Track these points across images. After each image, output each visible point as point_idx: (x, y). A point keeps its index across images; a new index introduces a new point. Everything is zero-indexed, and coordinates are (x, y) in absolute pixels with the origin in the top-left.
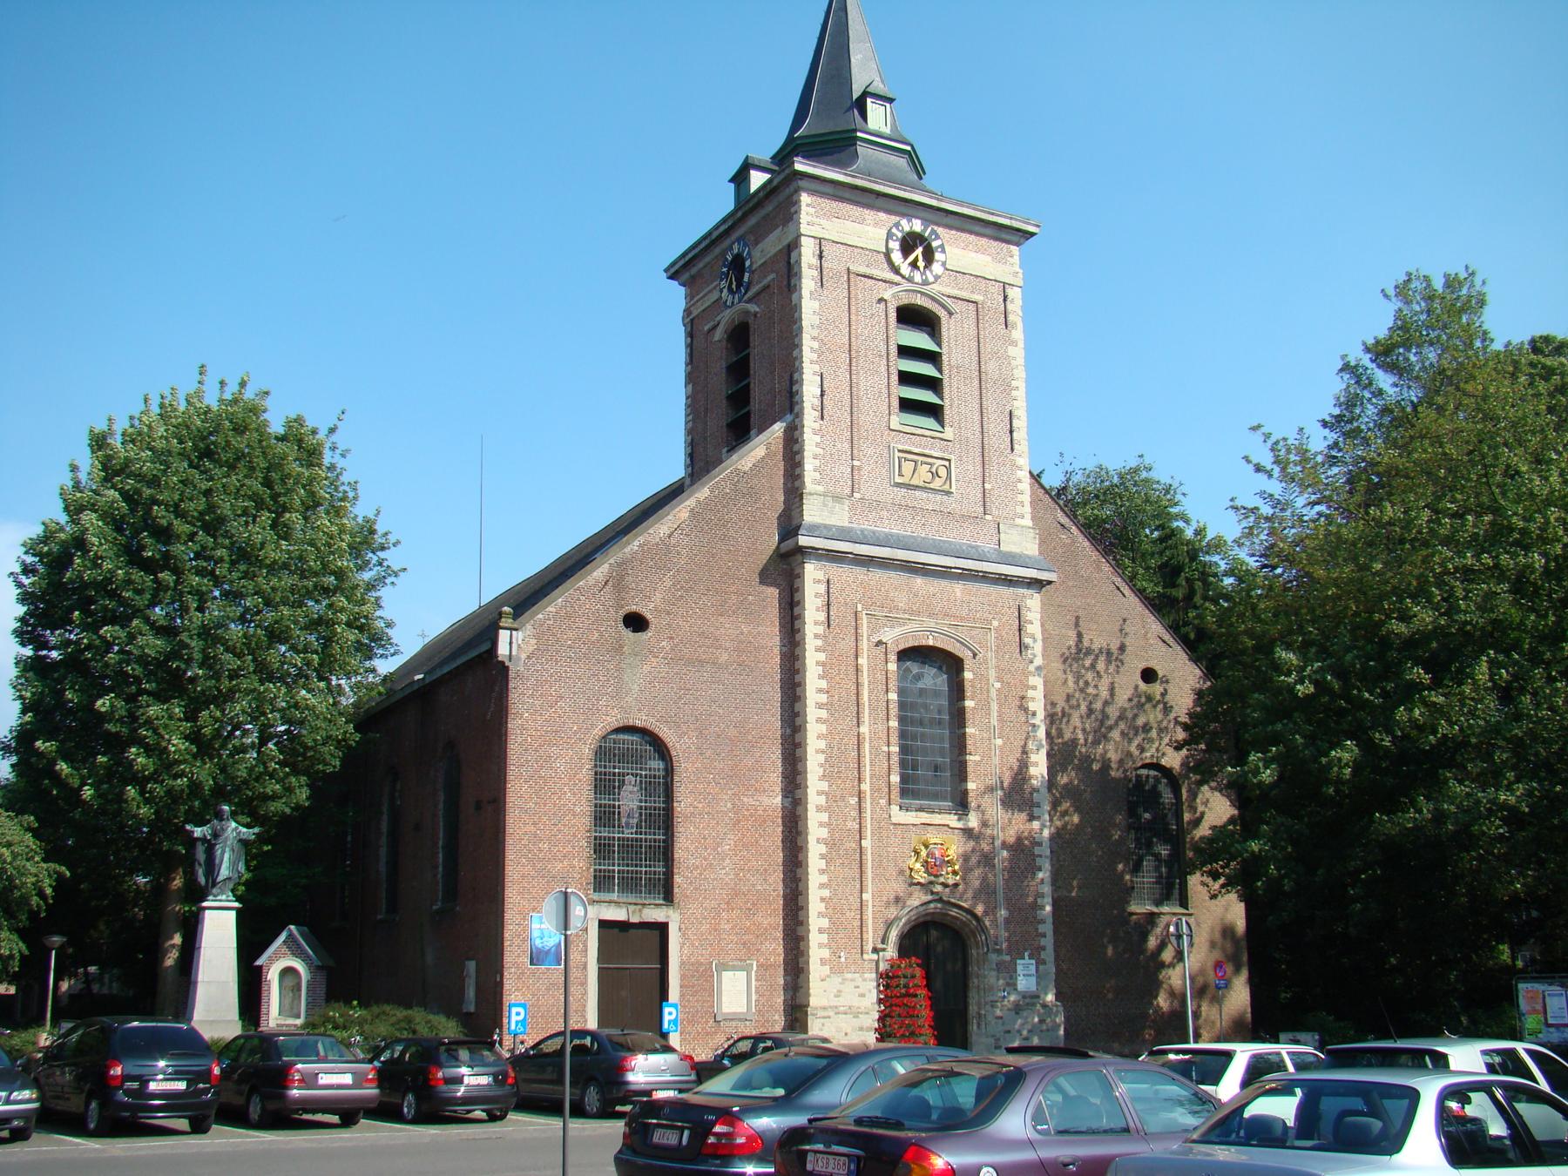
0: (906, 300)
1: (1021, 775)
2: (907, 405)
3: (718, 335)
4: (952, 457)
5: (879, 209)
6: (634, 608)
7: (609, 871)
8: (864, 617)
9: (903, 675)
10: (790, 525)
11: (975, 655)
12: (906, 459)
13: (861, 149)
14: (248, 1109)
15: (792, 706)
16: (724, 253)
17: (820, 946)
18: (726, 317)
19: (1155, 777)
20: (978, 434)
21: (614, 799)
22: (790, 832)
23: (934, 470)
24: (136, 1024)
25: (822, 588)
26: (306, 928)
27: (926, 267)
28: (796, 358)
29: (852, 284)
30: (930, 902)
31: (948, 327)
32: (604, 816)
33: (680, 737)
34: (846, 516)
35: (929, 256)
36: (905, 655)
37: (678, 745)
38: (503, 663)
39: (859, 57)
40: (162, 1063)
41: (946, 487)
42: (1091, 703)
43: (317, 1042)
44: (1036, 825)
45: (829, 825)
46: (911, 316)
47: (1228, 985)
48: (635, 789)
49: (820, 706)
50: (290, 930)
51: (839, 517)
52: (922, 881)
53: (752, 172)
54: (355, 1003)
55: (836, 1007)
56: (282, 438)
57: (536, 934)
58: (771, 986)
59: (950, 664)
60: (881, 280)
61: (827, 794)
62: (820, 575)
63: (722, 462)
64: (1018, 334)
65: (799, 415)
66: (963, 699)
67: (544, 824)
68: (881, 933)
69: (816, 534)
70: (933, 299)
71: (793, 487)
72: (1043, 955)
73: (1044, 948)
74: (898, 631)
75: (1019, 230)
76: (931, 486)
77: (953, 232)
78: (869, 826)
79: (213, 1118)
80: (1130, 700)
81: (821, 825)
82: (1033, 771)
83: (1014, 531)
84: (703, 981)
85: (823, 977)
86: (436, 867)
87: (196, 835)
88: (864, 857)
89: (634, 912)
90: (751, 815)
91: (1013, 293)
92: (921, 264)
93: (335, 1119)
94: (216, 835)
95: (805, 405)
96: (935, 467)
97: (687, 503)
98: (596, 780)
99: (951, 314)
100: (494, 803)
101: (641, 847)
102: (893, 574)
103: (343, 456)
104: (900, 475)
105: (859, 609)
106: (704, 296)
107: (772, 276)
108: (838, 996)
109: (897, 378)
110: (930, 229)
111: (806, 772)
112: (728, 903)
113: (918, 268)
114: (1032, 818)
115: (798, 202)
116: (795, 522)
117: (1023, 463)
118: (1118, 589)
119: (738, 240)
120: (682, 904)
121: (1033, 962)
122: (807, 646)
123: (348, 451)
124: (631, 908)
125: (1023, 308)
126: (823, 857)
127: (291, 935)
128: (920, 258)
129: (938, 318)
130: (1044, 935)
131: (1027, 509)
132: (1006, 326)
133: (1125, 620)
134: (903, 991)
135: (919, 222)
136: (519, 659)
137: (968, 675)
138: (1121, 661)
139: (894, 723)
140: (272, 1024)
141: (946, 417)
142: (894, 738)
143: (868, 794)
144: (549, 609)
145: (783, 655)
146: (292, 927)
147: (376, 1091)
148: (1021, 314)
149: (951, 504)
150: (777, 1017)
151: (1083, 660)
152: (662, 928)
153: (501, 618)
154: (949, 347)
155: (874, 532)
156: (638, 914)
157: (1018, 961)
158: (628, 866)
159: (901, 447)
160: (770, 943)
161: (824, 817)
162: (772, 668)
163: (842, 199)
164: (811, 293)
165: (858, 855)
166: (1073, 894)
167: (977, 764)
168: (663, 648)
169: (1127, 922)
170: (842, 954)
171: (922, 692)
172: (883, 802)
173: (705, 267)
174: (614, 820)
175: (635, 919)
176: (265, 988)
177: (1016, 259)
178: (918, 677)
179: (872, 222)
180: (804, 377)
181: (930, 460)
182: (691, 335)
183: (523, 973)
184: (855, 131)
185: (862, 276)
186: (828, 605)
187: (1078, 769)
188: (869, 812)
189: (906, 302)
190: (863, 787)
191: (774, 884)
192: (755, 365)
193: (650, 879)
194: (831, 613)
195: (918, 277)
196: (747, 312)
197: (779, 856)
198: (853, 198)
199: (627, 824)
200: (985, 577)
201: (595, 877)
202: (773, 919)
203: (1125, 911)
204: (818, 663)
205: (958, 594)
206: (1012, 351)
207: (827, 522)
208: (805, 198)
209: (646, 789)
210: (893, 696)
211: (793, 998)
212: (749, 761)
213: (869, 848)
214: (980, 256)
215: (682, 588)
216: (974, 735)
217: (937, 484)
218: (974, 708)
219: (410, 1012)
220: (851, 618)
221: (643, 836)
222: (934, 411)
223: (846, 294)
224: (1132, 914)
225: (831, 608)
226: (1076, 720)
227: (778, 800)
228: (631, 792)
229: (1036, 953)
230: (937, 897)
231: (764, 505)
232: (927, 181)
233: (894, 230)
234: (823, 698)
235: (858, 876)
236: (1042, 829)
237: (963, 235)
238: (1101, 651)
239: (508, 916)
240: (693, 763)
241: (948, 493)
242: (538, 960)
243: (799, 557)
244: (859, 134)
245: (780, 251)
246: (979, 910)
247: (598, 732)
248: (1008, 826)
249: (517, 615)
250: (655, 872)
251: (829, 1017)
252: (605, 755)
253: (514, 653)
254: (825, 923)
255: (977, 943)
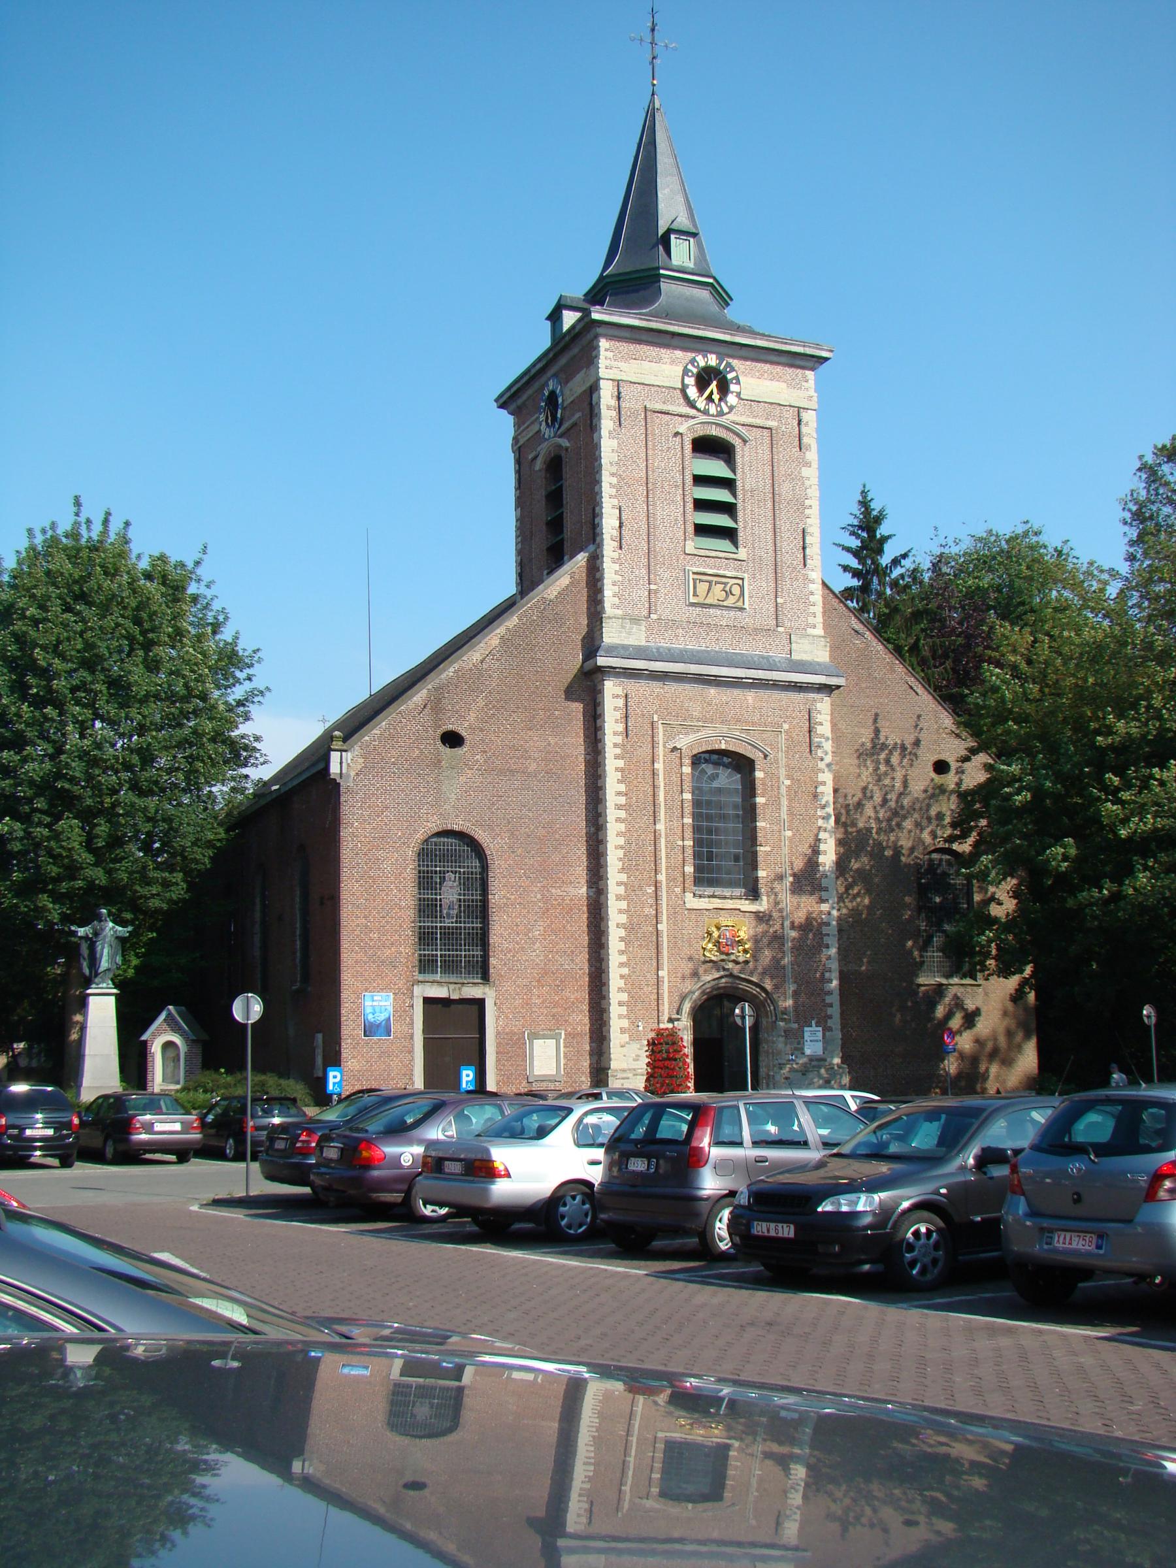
0: (701, 432)
1: (812, 863)
2: (702, 530)
3: (539, 465)
4: (746, 575)
5: (675, 348)
6: (450, 727)
7: (433, 955)
8: (660, 726)
9: (697, 776)
10: (591, 644)
11: (766, 756)
12: (701, 581)
13: (664, 286)
14: (105, 1150)
15: (596, 808)
16: (542, 388)
17: (620, 1016)
18: (544, 449)
19: (948, 861)
20: (771, 551)
21: (436, 894)
22: (595, 918)
23: (727, 589)
24: (50, 1089)
25: (621, 702)
26: (183, 1008)
27: (720, 400)
28: (597, 493)
29: (649, 420)
30: (721, 977)
31: (742, 455)
32: (427, 908)
33: (494, 839)
34: (643, 636)
35: (724, 389)
36: (697, 760)
37: (491, 845)
38: (335, 780)
39: (666, 191)
40: (39, 1116)
41: (740, 604)
42: (886, 794)
43: (159, 1100)
44: (825, 907)
45: (627, 911)
46: (706, 446)
47: (1019, 1048)
48: (455, 884)
49: (619, 807)
50: (168, 1009)
51: (637, 637)
52: (714, 958)
53: (564, 312)
54: (223, 1070)
55: (634, 1070)
56: (148, 576)
57: (369, 1010)
58: (578, 1051)
59: (742, 765)
60: (677, 415)
61: (625, 884)
62: (619, 691)
63: (543, 582)
64: (812, 455)
65: (600, 546)
66: (753, 795)
67: (374, 917)
68: (676, 1005)
69: (614, 654)
70: (728, 429)
71: (596, 611)
72: (830, 1023)
73: (830, 1017)
74: (692, 737)
75: (813, 356)
76: (725, 604)
77: (748, 363)
78: (665, 912)
79: (75, 1155)
80: (925, 791)
81: (620, 911)
82: (821, 859)
83: (805, 641)
84: (517, 1049)
85: (623, 1043)
86: (294, 953)
87: (79, 934)
88: (660, 939)
89: (454, 990)
90: (559, 905)
91: (809, 417)
92: (716, 397)
93: (173, 1158)
94: (96, 934)
95: (604, 536)
96: (729, 585)
97: (498, 631)
98: (420, 877)
99: (745, 441)
100: (331, 900)
101: (461, 934)
102: (687, 686)
103: (208, 586)
104: (695, 595)
105: (656, 719)
106: (527, 427)
107: (578, 415)
108: (638, 1060)
109: (692, 506)
110: (725, 362)
111: (607, 866)
112: (539, 981)
113: (712, 401)
114: (822, 901)
115: (596, 348)
116: (597, 643)
117: (816, 575)
118: (911, 688)
119: (555, 375)
120: (497, 982)
121: (820, 1029)
122: (607, 755)
123: (212, 582)
124: (452, 987)
125: (817, 430)
126: (622, 939)
127: (170, 1014)
128: (715, 391)
129: (733, 446)
130: (831, 1005)
131: (819, 619)
132: (800, 449)
133: (919, 717)
134: (665, 1056)
135: (714, 357)
136: (348, 776)
137: (759, 774)
138: (915, 755)
139: (688, 820)
140: (157, 1090)
141: (740, 539)
142: (689, 833)
143: (664, 883)
144: (375, 731)
145: (587, 762)
146: (171, 1007)
147: (199, 1136)
148: (815, 435)
149: (745, 619)
150: (583, 1079)
151: (878, 754)
152: (480, 1003)
153: (332, 741)
154: (743, 472)
155: (669, 650)
156: (458, 991)
157: (806, 1029)
158: (449, 950)
159: (695, 570)
160: (577, 1015)
161: (623, 905)
162: (577, 774)
163: (639, 342)
164: (610, 432)
165: (655, 937)
166: (864, 968)
167: (767, 854)
168: (477, 761)
169: (916, 993)
170: (640, 1024)
171: (719, 791)
172: (678, 890)
173: (528, 398)
174: (436, 912)
175: (455, 996)
176: (150, 1059)
177: (811, 383)
178: (714, 777)
179: (669, 361)
180: (604, 511)
181: (724, 580)
182: (518, 462)
183: (358, 1044)
184: (658, 268)
185: (658, 412)
186: (626, 717)
187: (871, 855)
188: (664, 899)
189: (701, 433)
190: (659, 877)
191: (581, 962)
192: (568, 497)
193: (469, 961)
194: (629, 724)
195: (713, 409)
196: (560, 446)
197: (585, 939)
198: (650, 340)
199: (448, 915)
200: (775, 685)
201: (420, 961)
202: (580, 994)
203: (912, 982)
204: (617, 769)
205: (750, 701)
206: (805, 472)
207: (626, 642)
208: (603, 344)
209: (464, 884)
210: (688, 796)
211: (599, 1061)
212: (556, 858)
213: (665, 930)
214: (775, 384)
215: (494, 707)
216: (765, 828)
217: (731, 601)
218: (765, 804)
219: (263, 1077)
220: (648, 727)
221: (462, 925)
222: (729, 534)
223: (643, 431)
224: (920, 985)
225: (629, 719)
226: (869, 811)
227: (584, 890)
228: (451, 887)
229: (823, 1021)
230: (727, 973)
231: (569, 628)
232: (732, 313)
233: (690, 367)
234: (622, 800)
235: (655, 955)
236: (828, 910)
237: (759, 365)
238: (895, 747)
239: (343, 995)
240: (506, 861)
241: (741, 609)
242: (370, 1032)
243: (599, 675)
244: (662, 272)
245: (585, 391)
246: (768, 985)
247: (420, 836)
248: (802, 907)
249: (345, 740)
250: (473, 955)
251: (628, 1078)
252: (427, 856)
253: (344, 771)
254: (624, 997)
255: (767, 1012)
